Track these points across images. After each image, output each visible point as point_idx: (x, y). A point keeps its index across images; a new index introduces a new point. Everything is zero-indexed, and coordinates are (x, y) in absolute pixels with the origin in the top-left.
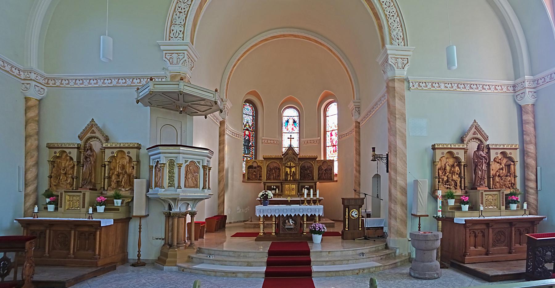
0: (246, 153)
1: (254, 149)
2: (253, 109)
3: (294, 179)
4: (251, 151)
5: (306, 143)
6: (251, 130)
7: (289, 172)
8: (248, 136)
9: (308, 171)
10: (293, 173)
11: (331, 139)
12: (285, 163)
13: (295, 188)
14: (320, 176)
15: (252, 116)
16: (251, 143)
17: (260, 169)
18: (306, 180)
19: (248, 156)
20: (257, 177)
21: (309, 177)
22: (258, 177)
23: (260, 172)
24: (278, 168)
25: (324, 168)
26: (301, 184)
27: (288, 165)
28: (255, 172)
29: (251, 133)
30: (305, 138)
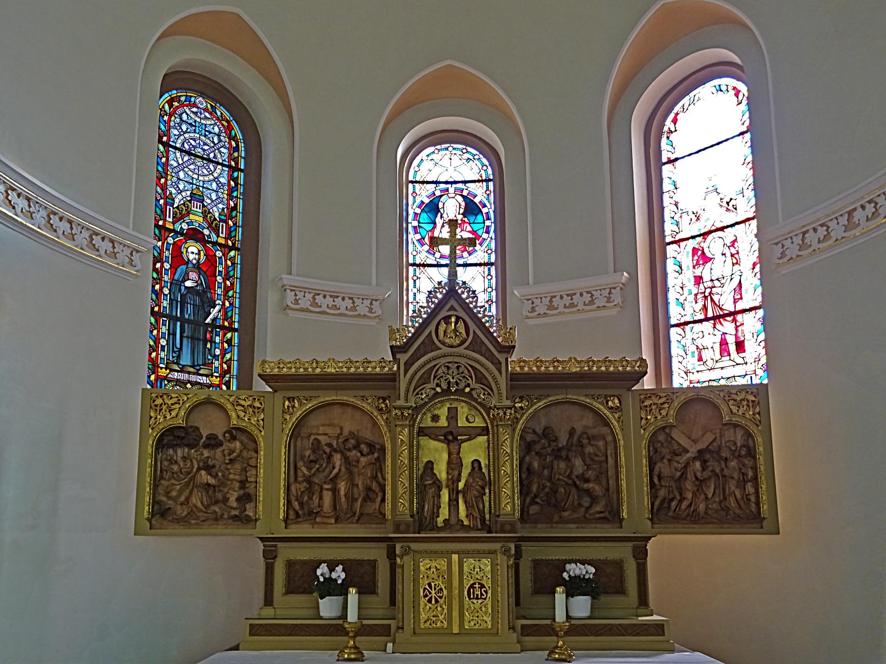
0: (186, 360)
1: (236, 341)
2: (237, 131)
3: (483, 519)
4: (218, 352)
5: (541, 309)
7: (441, 471)
8: (198, 267)
9: (578, 465)
11: (698, 280)
12: (417, 409)
13: (488, 584)
14: (662, 493)
15: (229, 166)
16: (218, 308)
17: (244, 446)
18: (562, 521)
19: (193, 378)
20: (226, 500)
21: (586, 501)
22: (233, 502)
23: (244, 470)
24: (371, 446)
25: (695, 441)
26: (531, 552)
27: (435, 418)
28: (208, 468)
29: (219, 254)
30: (536, 283)
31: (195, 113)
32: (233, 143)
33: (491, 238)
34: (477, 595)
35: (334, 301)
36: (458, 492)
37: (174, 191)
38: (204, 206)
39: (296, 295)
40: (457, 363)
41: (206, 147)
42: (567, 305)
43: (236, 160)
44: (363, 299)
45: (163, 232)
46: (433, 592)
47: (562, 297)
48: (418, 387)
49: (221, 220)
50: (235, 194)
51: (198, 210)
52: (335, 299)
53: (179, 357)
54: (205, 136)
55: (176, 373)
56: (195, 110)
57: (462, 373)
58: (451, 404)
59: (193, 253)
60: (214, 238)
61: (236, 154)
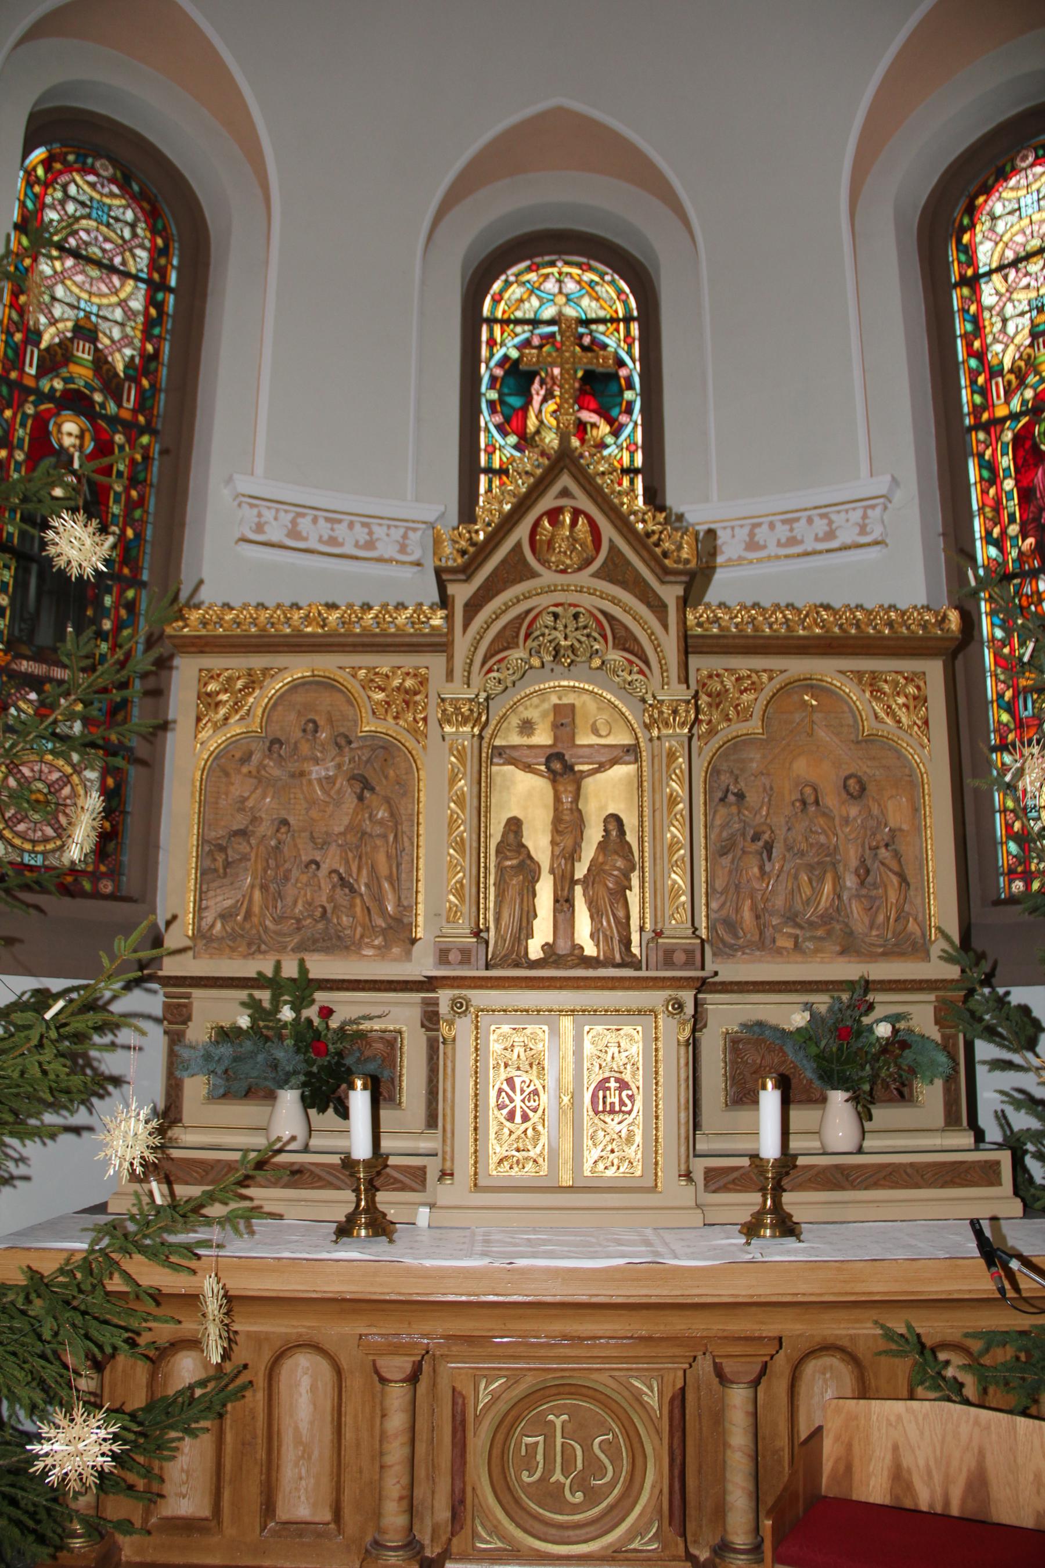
4: (107, 625)
6: (126, 415)
10: (602, 846)
13: (637, 1081)
29: (119, 438)
31: (93, 185)
32: (160, 242)
33: (636, 424)
34: (612, 1104)
35: (332, 529)
36: (574, 882)
37: (43, 320)
38: (97, 350)
39: (259, 515)
40: (576, 606)
41: (108, 246)
42: (783, 540)
43: (164, 275)
44: (389, 527)
45: (16, 394)
46: (518, 1098)
47: (772, 526)
48: (493, 656)
49: (127, 377)
50: (156, 331)
51: (86, 356)
52: (336, 526)
53: (32, 632)
54: (108, 225)
55: (25, 663)
56: (91, 178)
57: (585, 627)
58: (560, 698)
59: (70, 434)
60: (112, 408)
61: (163, 261)
